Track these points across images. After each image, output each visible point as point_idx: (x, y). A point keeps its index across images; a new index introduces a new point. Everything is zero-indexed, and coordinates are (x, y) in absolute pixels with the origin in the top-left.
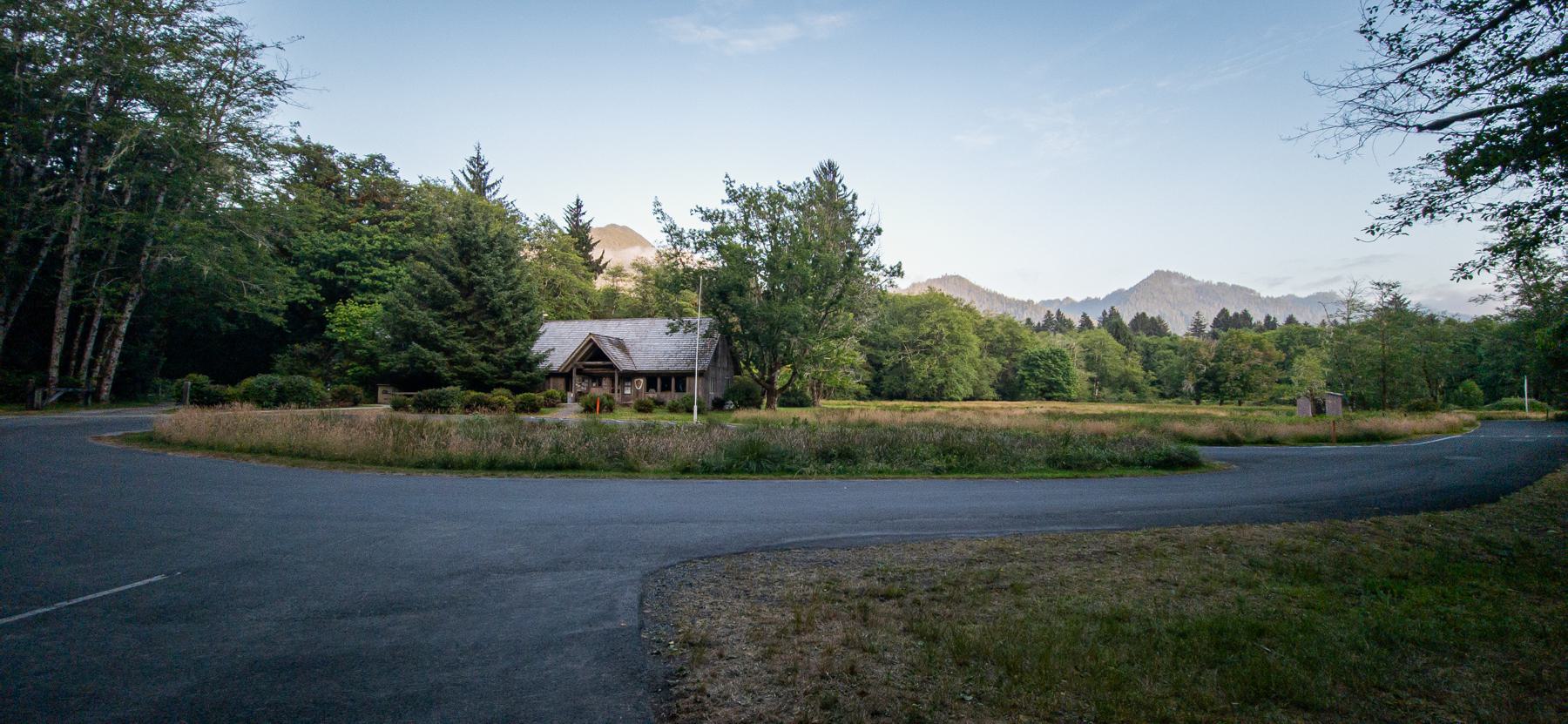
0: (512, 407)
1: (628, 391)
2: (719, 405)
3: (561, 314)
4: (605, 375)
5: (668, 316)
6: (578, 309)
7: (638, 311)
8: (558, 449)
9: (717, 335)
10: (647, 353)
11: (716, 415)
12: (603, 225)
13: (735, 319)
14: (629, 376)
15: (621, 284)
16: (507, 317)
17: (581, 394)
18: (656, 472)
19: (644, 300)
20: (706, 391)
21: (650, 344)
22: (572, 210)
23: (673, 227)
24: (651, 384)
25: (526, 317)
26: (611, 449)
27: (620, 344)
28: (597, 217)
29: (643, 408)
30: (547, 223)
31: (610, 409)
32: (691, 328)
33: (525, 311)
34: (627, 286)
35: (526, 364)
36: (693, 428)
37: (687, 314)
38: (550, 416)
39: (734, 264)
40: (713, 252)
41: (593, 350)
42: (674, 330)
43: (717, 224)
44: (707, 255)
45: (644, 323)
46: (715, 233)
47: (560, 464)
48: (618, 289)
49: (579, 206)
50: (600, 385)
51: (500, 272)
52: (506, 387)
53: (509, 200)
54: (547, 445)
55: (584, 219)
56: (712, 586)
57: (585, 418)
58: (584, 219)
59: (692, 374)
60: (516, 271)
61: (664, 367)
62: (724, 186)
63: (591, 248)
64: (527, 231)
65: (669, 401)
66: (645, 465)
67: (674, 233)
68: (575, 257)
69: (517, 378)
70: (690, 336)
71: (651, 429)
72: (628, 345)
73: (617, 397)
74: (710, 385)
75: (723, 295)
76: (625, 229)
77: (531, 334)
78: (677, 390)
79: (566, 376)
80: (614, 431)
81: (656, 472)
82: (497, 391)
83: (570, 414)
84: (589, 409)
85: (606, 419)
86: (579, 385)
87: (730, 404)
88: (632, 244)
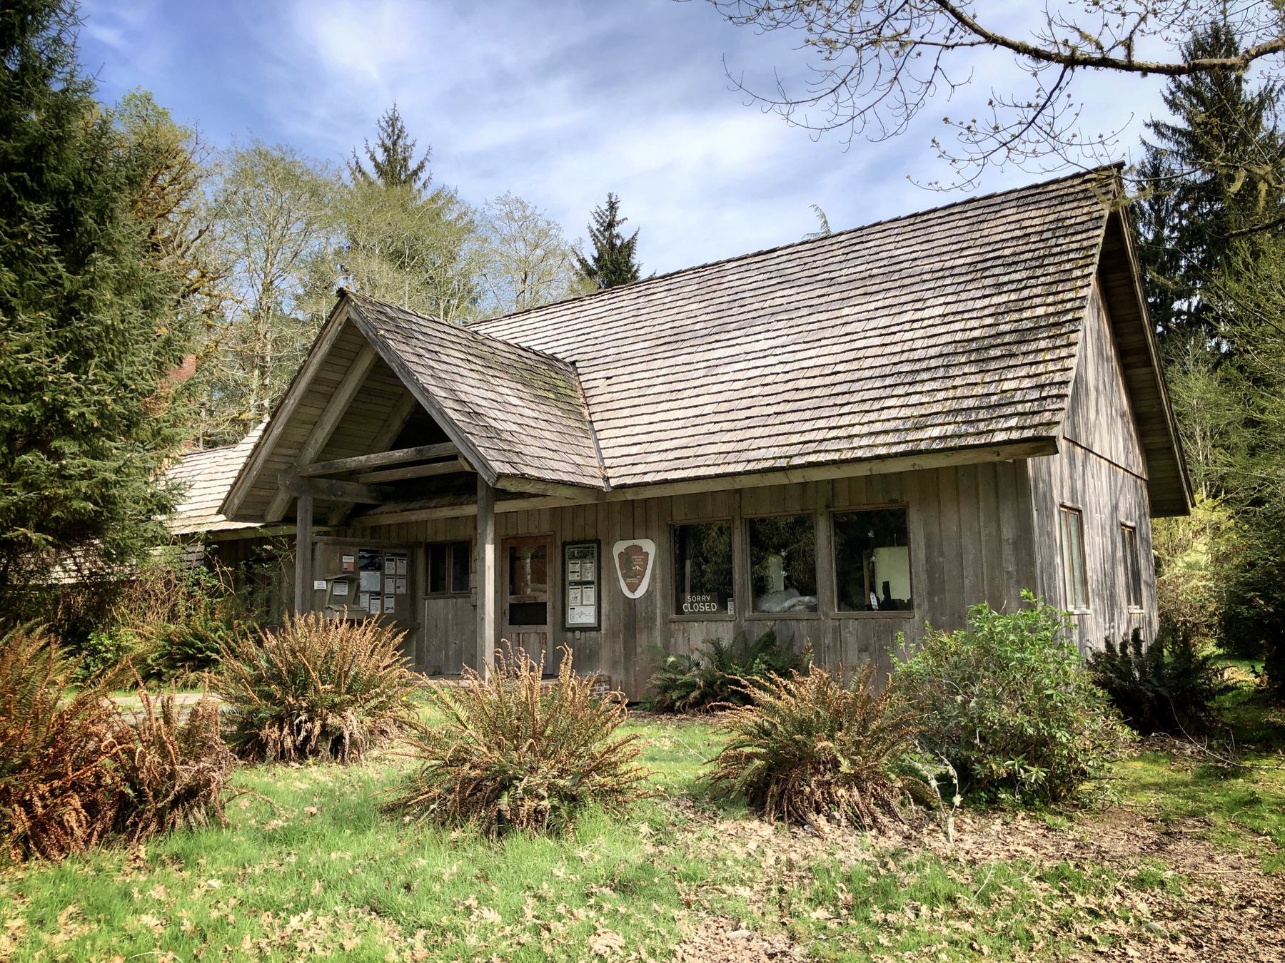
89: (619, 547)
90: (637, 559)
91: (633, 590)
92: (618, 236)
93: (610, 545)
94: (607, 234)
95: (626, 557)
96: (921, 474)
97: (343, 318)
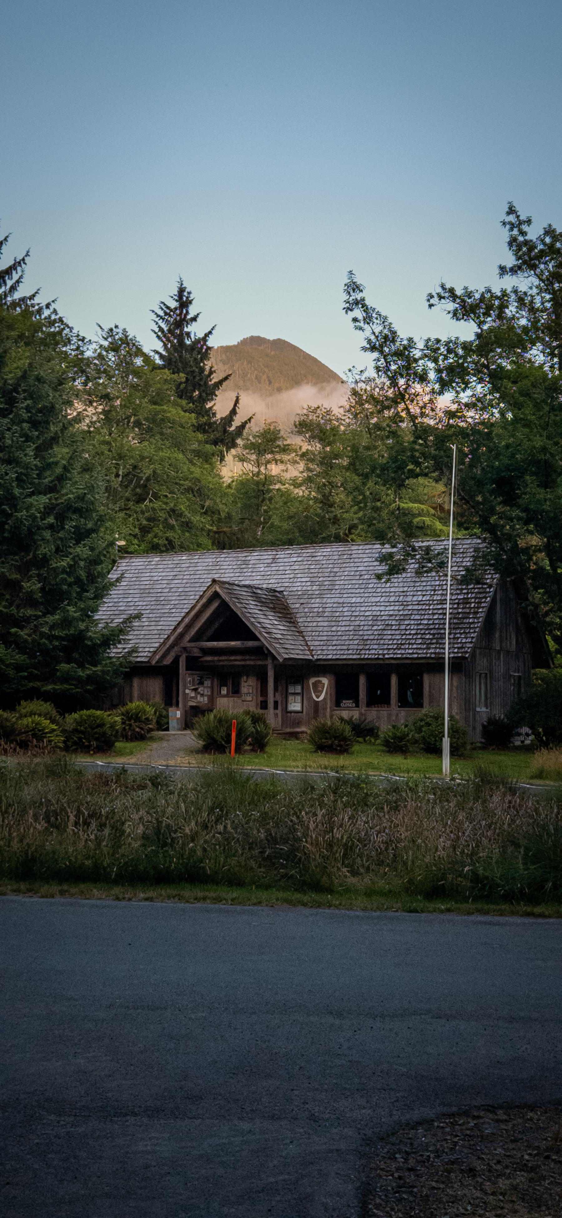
0: (59, 740)
1: (295, 706)
2: (497, 736)
3: (156, 540)
4: (246, 671)
5: (381, 537)
6: (187, 526)
7: (313, 529)
8: (159, 836)
9: (492, 578)
10: (334, 620)
11: (494, 762)
12: (233, 341)
13: (535, 540)
14: (297, 672)
15: (275, 470)
16: (44, 550)
17: (196, 711)
18: (369, 893)
19: (326, 502)
20: (468, 705)
21: (342, 598)
22: (168, 311)
23: (390, 337)
24: (345, 690)
25: (82, 550)
26: (272, 840)
27: (277, 603)
28: (221, 325)
29: (331, 742)
30: (121, 344)
31: (259, 744)
32: (433, 562)
33: (81, 535)
34: (287, 472)
35: (85, 647)
36: (444, 792)
37: (423, 530)
38: (135, 759)
39: (528, 411)
40: (479, 389)
41: (221, 617)
42: (395, 569)
43: (489, 323)
44: (465, 397)
45: (327, 553)
46: (485, 344)
47: (165, 870)
48: (269, 480)
49: (183, 300)
50: (236, 691)
51: (29, 456)
52: (46, 697)
53: (41, 300)
54: (135, 828)
55: (196, 330)
56: (521, 1178)
57: (209, 764)
58: (196, 330)
59: (435, 666)
60: (60, 452)
61: (373, 652)
62: (505, 235)
63: (210, 392)
64: (80, 365)
65: (385, 728)
66: (342, 874)
67: (389, 348)
68: (177, 412)
69: (66, 678)
70: (431, 580)
71: (353, 793)
72: (294, 604)
73: (272, 718)
74: (479, 691)
75: (506, 486)
76: (280, 345)
77: (92, 584)
78: (403, 702)
79: (163, 673)
80: (270, 796)
81: (369, 893)
82: (27, 706)
83: (174, 755)
84: (213, 745)
85: (251, 766)
86: (193, 693)
87: (525, 735)
88: (296, 382)
89: (312, 680)
90: (320, 685)
91: (318, 697)
92: (188, 334)
93: (308, 679)
94: (178, 331)
95: (315, 685)
96: (428, 664)
97: (213, 590)
